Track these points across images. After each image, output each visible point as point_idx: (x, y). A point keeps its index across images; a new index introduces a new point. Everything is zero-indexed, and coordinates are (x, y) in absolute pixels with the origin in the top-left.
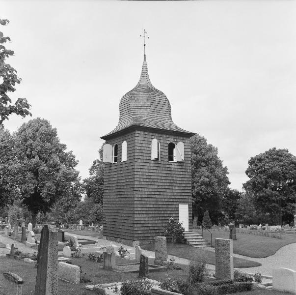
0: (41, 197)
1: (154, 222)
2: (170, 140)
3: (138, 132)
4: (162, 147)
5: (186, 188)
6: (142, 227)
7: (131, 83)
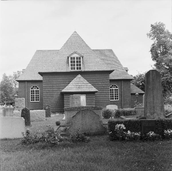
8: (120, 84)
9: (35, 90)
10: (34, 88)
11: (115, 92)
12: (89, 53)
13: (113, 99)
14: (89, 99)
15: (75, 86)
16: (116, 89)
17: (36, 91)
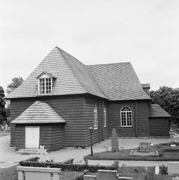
8: (133, 106)
9: (126, 112)
10: (125, 110)
11: (128, 116)
12: (65, 72)
13: (125, 125)
14: (43, 132)
15: (28, 116)
16: (129, 112)
17: (128, 113)
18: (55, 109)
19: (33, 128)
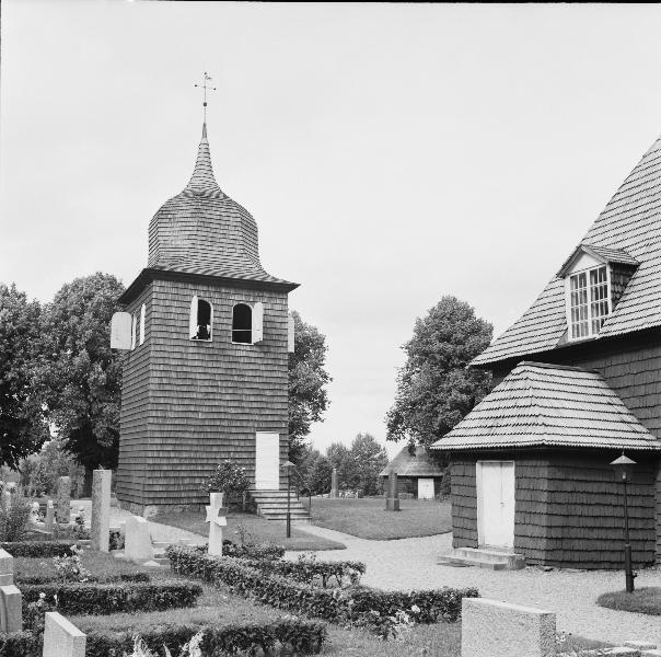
0: (95, 438)
1: (192, 468)
2: (238, 298)
3: (159, 283)
4: (218, 314)
5: (275, 399)
6: (165, 477)
7: (176, 181)
18: (625, 393)
19: (498, 469)
